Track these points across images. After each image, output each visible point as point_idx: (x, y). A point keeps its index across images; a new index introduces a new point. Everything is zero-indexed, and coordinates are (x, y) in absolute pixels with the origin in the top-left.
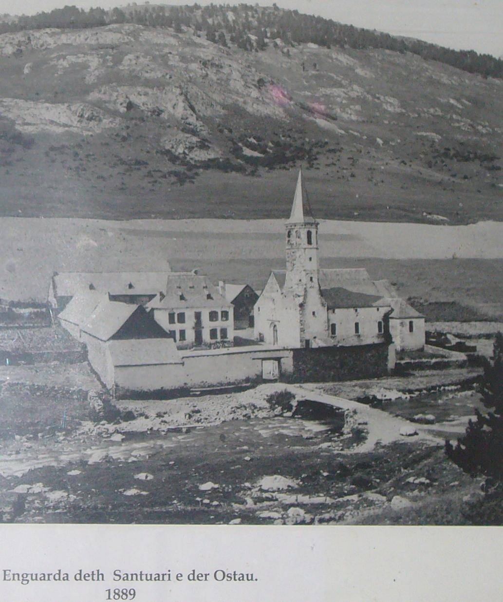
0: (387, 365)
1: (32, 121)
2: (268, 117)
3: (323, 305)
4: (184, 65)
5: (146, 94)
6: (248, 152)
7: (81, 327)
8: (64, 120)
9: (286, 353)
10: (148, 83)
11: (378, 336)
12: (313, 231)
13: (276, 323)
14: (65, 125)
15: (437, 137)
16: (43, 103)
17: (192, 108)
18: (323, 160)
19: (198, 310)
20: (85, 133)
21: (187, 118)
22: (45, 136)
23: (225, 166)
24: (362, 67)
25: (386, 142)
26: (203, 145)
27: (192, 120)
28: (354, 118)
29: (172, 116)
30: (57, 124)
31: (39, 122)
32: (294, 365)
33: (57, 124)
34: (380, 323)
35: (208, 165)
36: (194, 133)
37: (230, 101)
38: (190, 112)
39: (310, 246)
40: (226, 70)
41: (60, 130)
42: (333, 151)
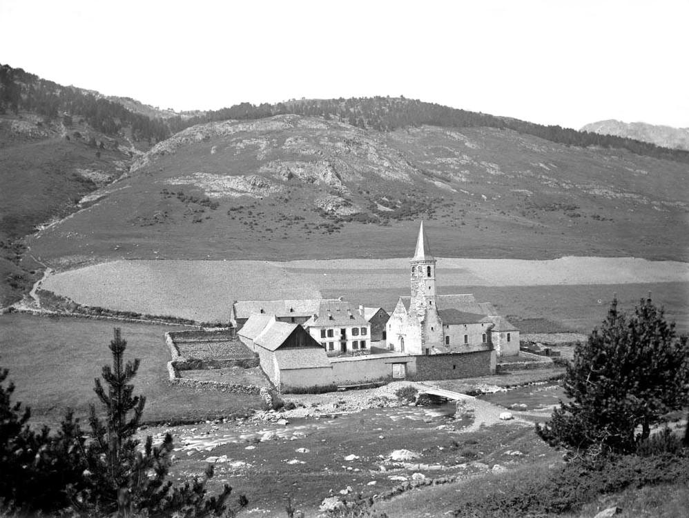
0: (489, 367)
1: (217, 188)
2: (396, 181)
3: (440, 322)
5: (303, 167)
6: (381, 208)
7: (254, 341)
8: (241, 188)
10: (305, 159)
11: (483, 345)
12: (432, 266)
13: (403, 336)
14: (242, 192)
15: (529, 193)
16: (225, 175)
17: (338, 176)
18: (439, 212)
22: (227, 200)
24: (471, 141)
26: (347, 204)
28: (464, 180)
29: (322, 183)
30: (237, 191)
33: (237, 191)
34: (484, 335)
35: (350, 219)
36: (340, 195)
37: (368, 170)
38: (336, 179)
39: (429, 278)
40: (365, 147)
41: (238, 195)
42: (447, 205)
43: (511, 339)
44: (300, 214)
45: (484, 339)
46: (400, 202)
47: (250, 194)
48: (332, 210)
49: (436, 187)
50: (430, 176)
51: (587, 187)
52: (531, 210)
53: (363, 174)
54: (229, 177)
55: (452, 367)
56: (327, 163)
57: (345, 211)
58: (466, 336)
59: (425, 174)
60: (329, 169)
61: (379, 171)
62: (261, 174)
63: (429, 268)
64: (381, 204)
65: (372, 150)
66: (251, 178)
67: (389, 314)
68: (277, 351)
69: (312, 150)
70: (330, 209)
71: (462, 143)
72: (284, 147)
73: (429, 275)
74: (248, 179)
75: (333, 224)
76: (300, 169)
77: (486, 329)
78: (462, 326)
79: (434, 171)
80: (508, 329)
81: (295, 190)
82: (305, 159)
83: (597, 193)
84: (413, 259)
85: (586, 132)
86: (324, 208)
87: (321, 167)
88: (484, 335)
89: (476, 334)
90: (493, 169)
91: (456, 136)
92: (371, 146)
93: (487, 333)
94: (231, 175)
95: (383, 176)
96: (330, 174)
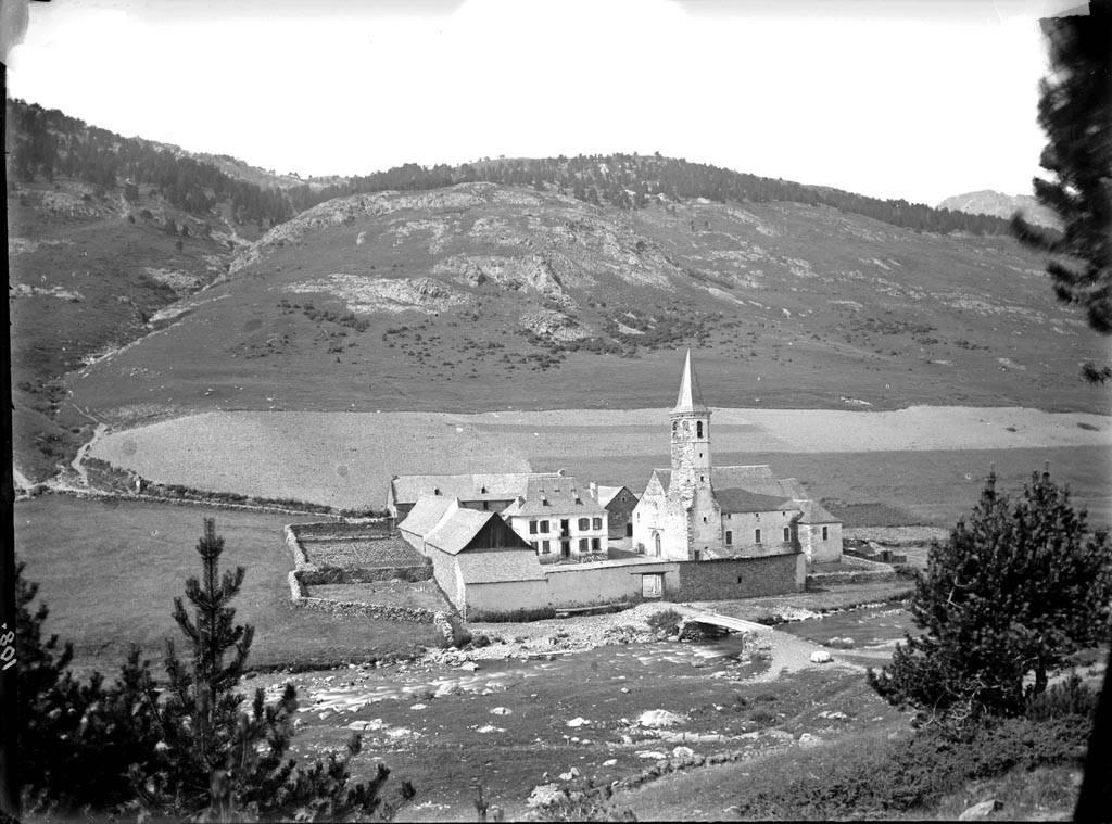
0: (794, 580)
3: (716, 509)
4: (547, 229)
5: (502, 265)
6: (625, 329)
7: (425, 538)
8: (404, 297)
9: (672, 567)
10: (504, 252)
11: (784, 545)
12: (704, 421)
13: (659, 532)
14: (405, 304)
16: (379, 278)
17: (557, 279)
18: (716, 336)
19: (565, 518)
20: (429, 312)
21: (551, 292)
22: (382, 316)
23: (598, 348)
24: (766, 225)
25: (795, 313)
26: (571, 323)
27: (557, 293)
28: (754, 285)
29: (532, 290)
30: (398, 303)
31: (375, 301)
32: (681, 581)
33: (398, 303)
34: (786, 530)
35: (576, 346)
36: (559, 308)
38: (555, 284)
39: (701, 440)
40: (598, 233)
41: (400, 309)
43: (829, 535)
44: (497, 338)
45: (786, 535)
46: (654, 320)
47: (418, 308)
48: (547, 332)
49: (711, 297)
50: (702, 278)
51: (949, 296)
52: (859, 333)
53: (596, 277)
54: (385, 280)
55: (735, 580)
56: (540, 260)
57: (567, 335)
58: (758, 532)
59: (693, 276)
60: (543, 269)
61: (621, 271)
62: (435, 276)
63: (699, 424)
64: (624, 323)
65: (609, 238)
66: (420, 282)
67: (637, 496)
68: (466, 555)
69: (516, 239)
70: (544, 331)
71: (752, 227)
72: (471, 234)
73: (700, 435)
74: (415, 283)
75: (549, 356)
76: (497, 268)
77: (789, 520)
78: (752, 515)
79: (708, 272)
80: (824, 520)
81: (489, 301)
82: (504, 252)
83: (963, 305)
84: (675, 411)
85: (946, 210)
86: (535, 330)
87: (530, 265)
88: (786, 530)
89: (774, 528)
90: (801, 268)
91: (742, 217)
92: (609, 232)
93: (790, 526)
94: (387, 278)
95: (627, 279)
96: (544, 275)
